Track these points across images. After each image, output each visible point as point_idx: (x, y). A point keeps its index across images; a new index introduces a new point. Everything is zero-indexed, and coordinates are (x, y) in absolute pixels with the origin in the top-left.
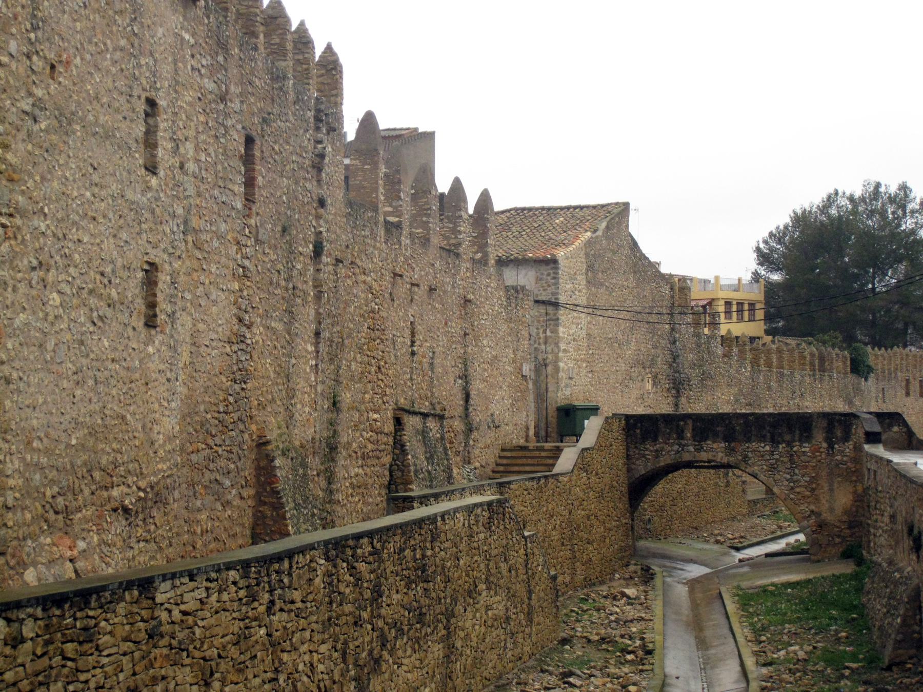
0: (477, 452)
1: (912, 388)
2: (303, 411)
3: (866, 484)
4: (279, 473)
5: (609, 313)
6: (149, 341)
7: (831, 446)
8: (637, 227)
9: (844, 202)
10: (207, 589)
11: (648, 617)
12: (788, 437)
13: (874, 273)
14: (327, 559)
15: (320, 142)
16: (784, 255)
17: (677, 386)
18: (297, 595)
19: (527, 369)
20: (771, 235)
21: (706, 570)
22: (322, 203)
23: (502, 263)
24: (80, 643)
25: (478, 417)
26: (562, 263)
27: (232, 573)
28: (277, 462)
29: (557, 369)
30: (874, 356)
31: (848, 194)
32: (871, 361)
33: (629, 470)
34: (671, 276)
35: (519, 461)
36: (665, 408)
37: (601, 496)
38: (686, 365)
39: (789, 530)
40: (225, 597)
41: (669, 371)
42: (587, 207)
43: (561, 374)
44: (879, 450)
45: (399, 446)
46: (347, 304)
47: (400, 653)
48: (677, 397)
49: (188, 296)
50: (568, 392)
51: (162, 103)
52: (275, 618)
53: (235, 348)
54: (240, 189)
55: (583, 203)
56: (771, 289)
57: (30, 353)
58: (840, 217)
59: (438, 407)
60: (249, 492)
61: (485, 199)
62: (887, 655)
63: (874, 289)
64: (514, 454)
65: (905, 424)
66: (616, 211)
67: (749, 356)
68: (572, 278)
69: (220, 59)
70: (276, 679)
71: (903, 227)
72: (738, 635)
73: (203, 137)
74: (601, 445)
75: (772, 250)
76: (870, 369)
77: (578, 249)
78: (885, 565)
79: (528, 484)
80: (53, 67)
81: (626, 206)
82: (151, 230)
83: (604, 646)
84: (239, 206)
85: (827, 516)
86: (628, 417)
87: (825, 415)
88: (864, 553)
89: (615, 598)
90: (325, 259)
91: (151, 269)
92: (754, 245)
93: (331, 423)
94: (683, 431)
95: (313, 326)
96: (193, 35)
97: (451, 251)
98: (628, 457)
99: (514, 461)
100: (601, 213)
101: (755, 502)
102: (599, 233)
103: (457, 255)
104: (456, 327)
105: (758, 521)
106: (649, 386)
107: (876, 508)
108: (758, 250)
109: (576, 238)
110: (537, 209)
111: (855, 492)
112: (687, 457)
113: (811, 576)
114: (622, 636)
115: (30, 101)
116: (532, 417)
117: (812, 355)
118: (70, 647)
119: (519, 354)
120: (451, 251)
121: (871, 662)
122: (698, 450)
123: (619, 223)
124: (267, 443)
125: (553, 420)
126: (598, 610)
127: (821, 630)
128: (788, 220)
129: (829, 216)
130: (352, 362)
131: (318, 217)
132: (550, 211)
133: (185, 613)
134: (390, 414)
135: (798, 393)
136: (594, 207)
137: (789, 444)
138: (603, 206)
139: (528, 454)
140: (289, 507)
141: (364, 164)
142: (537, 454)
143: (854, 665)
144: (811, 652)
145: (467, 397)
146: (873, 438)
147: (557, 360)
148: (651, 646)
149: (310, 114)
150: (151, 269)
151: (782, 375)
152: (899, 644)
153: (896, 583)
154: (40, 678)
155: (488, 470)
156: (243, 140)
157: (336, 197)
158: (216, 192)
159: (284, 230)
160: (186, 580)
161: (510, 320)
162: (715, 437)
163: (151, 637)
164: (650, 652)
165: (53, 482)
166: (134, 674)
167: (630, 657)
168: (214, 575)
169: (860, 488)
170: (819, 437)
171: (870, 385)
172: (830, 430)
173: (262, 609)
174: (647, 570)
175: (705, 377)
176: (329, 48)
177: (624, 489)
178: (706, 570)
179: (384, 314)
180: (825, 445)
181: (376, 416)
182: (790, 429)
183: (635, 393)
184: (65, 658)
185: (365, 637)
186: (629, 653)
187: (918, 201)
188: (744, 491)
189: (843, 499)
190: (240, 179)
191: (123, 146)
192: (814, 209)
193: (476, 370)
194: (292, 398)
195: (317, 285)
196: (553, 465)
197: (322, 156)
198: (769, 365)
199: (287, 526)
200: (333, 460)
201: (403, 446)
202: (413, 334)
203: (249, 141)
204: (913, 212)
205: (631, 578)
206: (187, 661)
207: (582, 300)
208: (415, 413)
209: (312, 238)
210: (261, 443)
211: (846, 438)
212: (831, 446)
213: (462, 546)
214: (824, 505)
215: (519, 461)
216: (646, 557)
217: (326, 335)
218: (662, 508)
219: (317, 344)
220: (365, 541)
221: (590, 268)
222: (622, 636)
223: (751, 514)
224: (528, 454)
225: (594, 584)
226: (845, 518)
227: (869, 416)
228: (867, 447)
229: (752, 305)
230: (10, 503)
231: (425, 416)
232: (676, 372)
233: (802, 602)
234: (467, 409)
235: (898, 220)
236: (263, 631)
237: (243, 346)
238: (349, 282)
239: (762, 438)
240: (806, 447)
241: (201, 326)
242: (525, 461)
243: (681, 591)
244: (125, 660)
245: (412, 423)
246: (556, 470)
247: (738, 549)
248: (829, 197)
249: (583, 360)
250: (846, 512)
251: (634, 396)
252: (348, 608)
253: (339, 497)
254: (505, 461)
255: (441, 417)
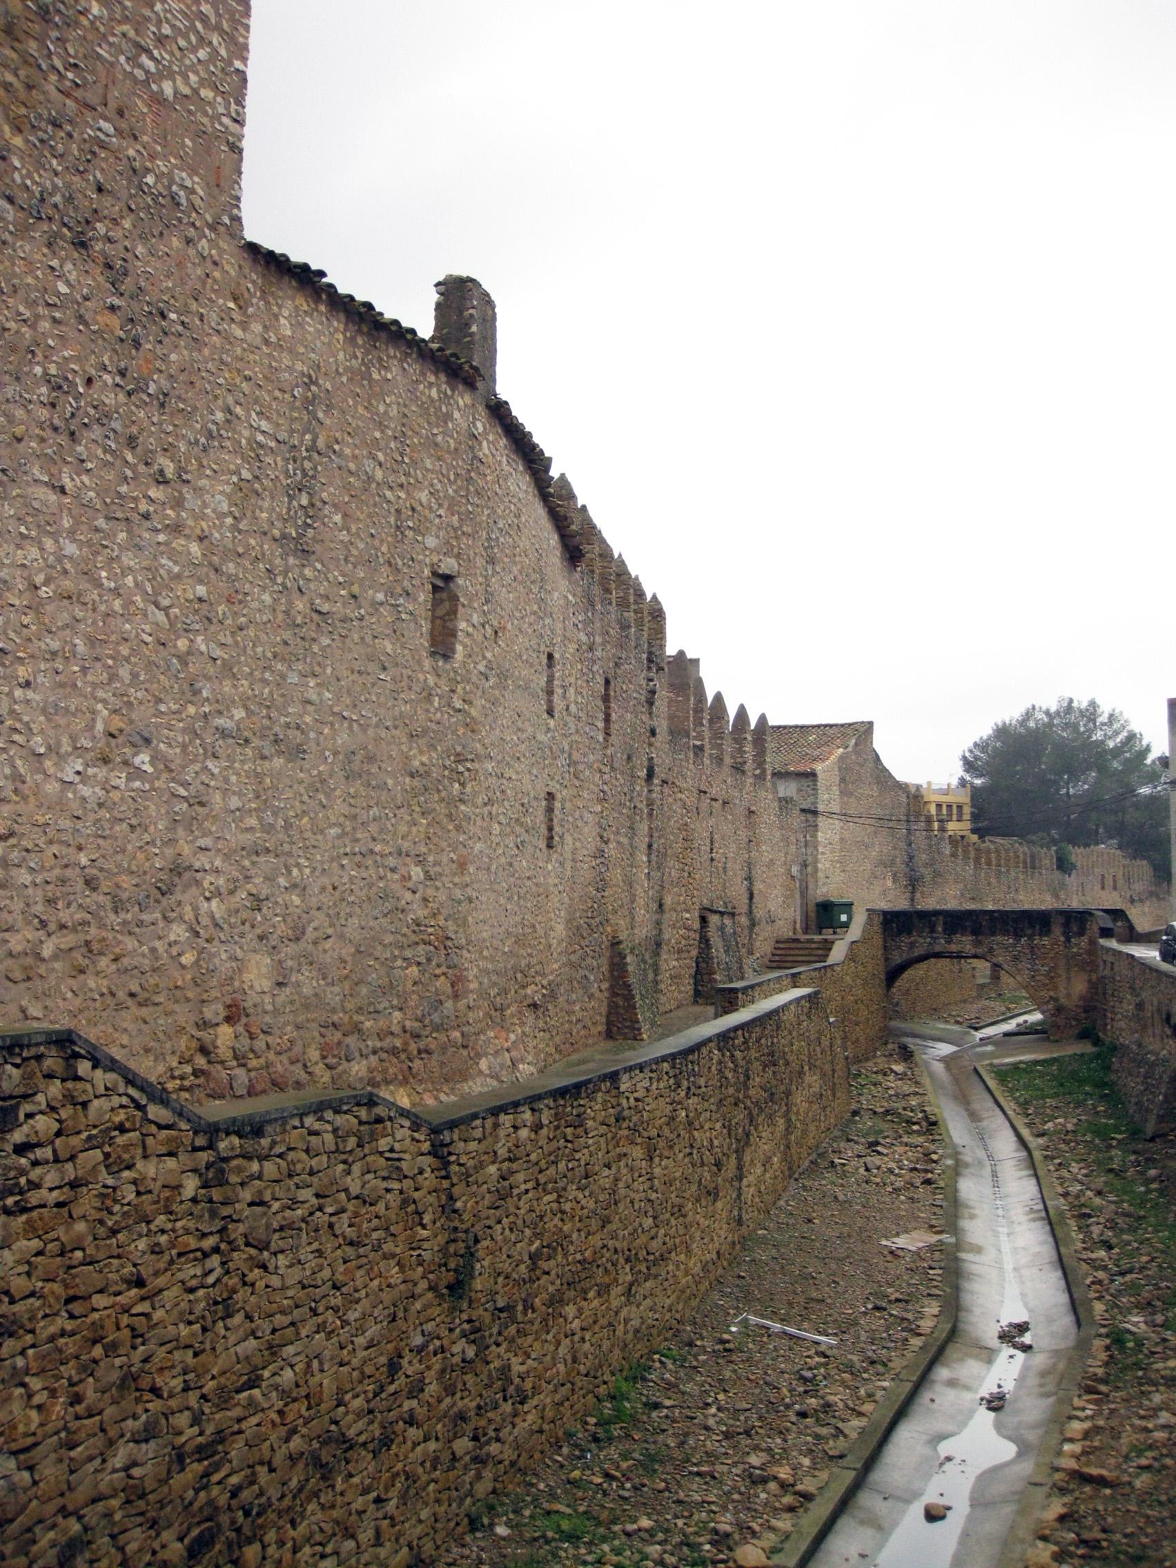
0: (758, 943)
1: (1106, 883)
2: (641, 913)
3: (1101, 974)
4: (630, 968)
5: (857, 820)
6: (549, 860)
7: (1068, 940)
8: (881, 743)
9: (1040, 716)
10: (651, 1078)
11: (920, 1091)
12: (1029, 932)
13: (1069, 779)
14: (719, 1050)
15: (651, 680)
16: (987, 763)
17: (913, 883)
18: (702, 1081)
19: (795, 870)
20: (976, 745)
21: (954, 1048)
22: (653, 733)
23: (777, 775)
24: (575, 1127)
25: (759, 913)
26: (820, 776)
27: (665, 1064)
28: (629, 959)
29: (816, 870)
30: (1077, 854)
31: (1044, 708)
32: (1073, 859)
33: (887, 960)
34: (907, 785)
35: (792, 952)
36: (902, 904)
37: (865, 983)
38: (920, 863)
39: (1016, 1012)
40: (662, 1085)
41: (907, 870)
42: (836, 725)
43: (820, 874)
44: (1113, 944)
45: (705, 941)
46: (669, 819)
47: (761, 1128)
48: (913, 892)
49: (571, 819)
50: (824, 890)
51: (557, 656)
52: (690, 1101)
53: (598, 861)
54: (601, 725)
55: (832, 722)
56: (976, 793)
57: (482, 876)
58: (1037, 728)
59: (730, 906)
60: (605, 985)
61: (763, 719)
62: (1150, 1128)
63: (1068, 792)
64: (787, 945)
65: (1128, 920)
66: (862, 729)
67: (972, 854)
68: (829, 788)
69: (590, 614)
70: (691, 1154)
71: (1094, 738)
72: (1006, 1108)
73: (579, 682)
74: (865, 940)
75: (976, 758)
76: (1074, 867)
77: (834, 763)
78: (1134, 1047)
79: (813, 974)
80: (496, 632)
81: (871, 724)
82: (551, 765)
83: (889, 1117)
84: (601, 739)
85: (1063, 1001)
86: (885, 913)
87: (1061, 913)
88: (1100, 1034)
89: (885, 1074)
90: (656, 781)
91: (550, 796)
92: (960, 754)
93: (658, 923)
94: (934, 926)
95: (647, 839)
96: (574, 595)
97: (738, 769)
98: (885, 948)
99: (788, 952)
100: (849, 731)
101: (982, 986)
102: (850, 749)
103: (743, 772)
104: (743, 834)
105: (987, 1003)
106: (889, 883)
107: (1113, 995)
108: (964, 758)
109: (830, 753)
110: (791, 727)
111: (1090, 981)
112: (938, 949)
113: (1055, 1055)
114: (905, 1109)
115: (484, 662)
116: (798, 913)
117: (1025, 854)
118: (569, 1130)
119: (789, 857)
120: (738, 769)
121: (1134, 1134)
122: (949, 942)
123: (866, 740)
124: (619, 943)
125: (813, 915)
126: (875, 1085)
127: (1078, 1104)
128: (991, 732)
129: (1027, 729)
130: (673, 869)
131: (651, 745)
132: (803, 729)
133: (637, 1100)
134: (697, 914)
135: (1013, 888)
136: (842, 725)
137: (1031, 937)
138: (850, 725)
139: (800, 945)
140: (638, 997)
141: (678, 696)
142: (808, 945)
143: (1119, 1137)
144: (1077, 1124)
145: (751, 897)
146: (1106, 933)
147: (816, 861)
148: (933, 1118)
149: (645, 656)
150: (550, 796)
151: (1000, 872)
152: (1161, 1118)
153: (1152, 1065)
154: (552, 1158)
155: (766, 960)
156: (603, 682)
157: (662, 726)
158: (587, 729)
159: (629, 758)
160: (637, 1072)
161: (782, 828)
162: (964, 931)
163: (617, 1121)
164: (935, 1124)
165: (495, 984)
166: (608, 1152)
167: (915, 1127)
168: (654, 1067)
169: (1094, 977)
170: (1057, 931)
171: (1072, 880)
172: (1067, 925)
173: (683, 1094)
174: (904, 1048)
175: (937, 874)
176: (654, 597)
177: (883, 977)
178: (954, 1048)
179: (692, 826)
180: (1062, 939)
181: (688, 915)
182: (1032, 926)
183: (878, 890)
184: (567, 1141)
185: (740, 1116)
186: (914, 1124)
187: (1106, 715)
188: (974, 976)
189: (1079, 986)
190: (601, 716)
191: (534, 695)
192: (1014, 722)
193: (758, 872)
194: (633, 903)
195: (650, 804)
196: (827, 956)
197: (653, 692)
198: (989, 864)
199: (636, 1014)
200: (658, 955)
201: (707, 940)
202: (712, 843)
203: (607, 682)
204: (1103, 724)
205: (891, 1055)
206: (639, 1140)
207: (836, 809)
208: (716, 912)
209: (646, 764)
210: (615, 943)
211: (1081, 933)
212: (1068, 940)
213: (794, 1034)
214: (1062, 992)
215: (792, 952)
216: (899, 1036)
217: (655, 846)
218: (907, 992)
219: (649, 855)
220: (740, 1033)
221: (843, 780)
222: (905, 1109)
223: (979, 997)
224: (800, 945)
225: (860, 1061)
226: (1081, 1003)
227: (1101, 913)
228: (1102, 941)
229: (960, 807)
230: (472, 1004)
231: (722, 914)
232: (912, 870)
233: (1055, 1078)
234: (750, 906)
235: (1091, 732)
236: (684, 1114)
237: (602, 860)
238: (670, 800)
239: (1006, 933)
240: (1046, 941)
241: (578, 844)
242: (797, 952)
243: (938, 1068)
244: (602, 1140)
245: (714, 919)
246: (830, 961)
247: (976, 1029)
248: (1027, 714)
249: (838, 861)
250: (1082, 998)
251: (877, 892)
252: (731, 1091)
253: (662, 986)
254: (779, 952)
255: (733, 915)
